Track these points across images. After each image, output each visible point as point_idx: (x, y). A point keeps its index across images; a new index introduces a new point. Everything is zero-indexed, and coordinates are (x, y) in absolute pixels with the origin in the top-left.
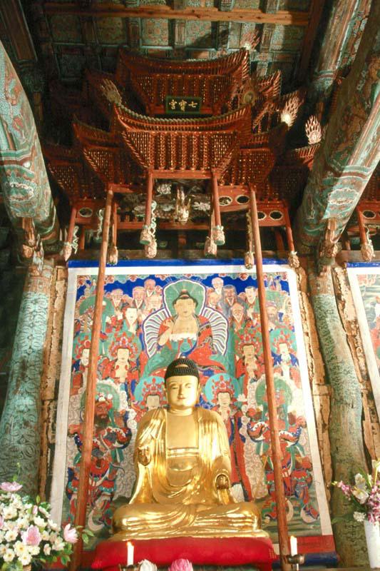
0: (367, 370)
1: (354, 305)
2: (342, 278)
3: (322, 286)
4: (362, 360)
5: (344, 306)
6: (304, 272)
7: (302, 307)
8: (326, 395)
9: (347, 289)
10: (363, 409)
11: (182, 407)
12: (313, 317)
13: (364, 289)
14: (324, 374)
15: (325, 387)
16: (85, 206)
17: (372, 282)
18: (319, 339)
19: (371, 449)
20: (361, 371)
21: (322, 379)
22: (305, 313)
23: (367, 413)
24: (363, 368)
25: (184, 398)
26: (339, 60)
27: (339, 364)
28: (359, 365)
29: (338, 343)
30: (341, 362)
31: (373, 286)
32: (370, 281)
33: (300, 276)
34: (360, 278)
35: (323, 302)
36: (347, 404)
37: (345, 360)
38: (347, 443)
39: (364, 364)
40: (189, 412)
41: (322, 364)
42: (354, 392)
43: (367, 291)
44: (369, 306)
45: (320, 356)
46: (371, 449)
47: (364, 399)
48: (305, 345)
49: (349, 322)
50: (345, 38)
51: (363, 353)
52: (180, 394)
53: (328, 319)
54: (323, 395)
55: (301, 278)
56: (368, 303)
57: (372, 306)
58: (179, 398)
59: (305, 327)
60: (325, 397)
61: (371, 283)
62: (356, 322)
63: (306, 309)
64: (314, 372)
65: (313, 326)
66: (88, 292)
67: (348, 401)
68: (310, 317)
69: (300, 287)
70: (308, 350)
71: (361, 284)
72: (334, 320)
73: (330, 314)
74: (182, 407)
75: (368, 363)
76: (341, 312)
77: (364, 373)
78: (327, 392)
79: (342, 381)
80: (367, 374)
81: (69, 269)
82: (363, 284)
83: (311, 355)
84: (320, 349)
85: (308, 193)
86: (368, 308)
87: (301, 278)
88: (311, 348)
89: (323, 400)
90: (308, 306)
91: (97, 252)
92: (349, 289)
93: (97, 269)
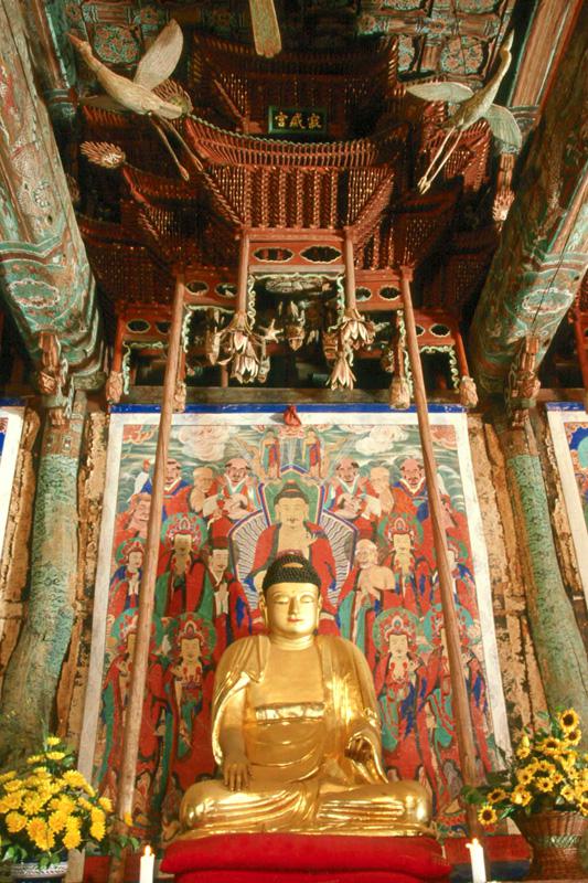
0: (94, 581)
1: (104, 474)
2: (97, 431)
3: (54, 442)
4: (91, 564)
5: (87, 476)
6: (38, 421)
7: (18, 475)
8: (17, 618)
9: (102, 449)
10: (70, 643)
11: (292, 635)
12: (33, 492)
13: (129, 448)
14: (24, 585)
15: (20, 606)
16: (139, 316)
17: (147, 437)
18: (32, 529)
19: (64, 709)
20: (86, 581)
21: (19, 592)
22: (21, 484)
23: (76, 651)
24: (90, 577)
25: (297, 620)
26: (64, 71)
27: (42, 569)
28: (84, 571)
29: (52, 532)
30: (46, 565)
31: (146, 444)
32: (143, 435)
33: (32, 425)
34: (129, 430)
35: (49, 468)
36: (36, 633)
37: (53, 563)
38: (17, 698)
39: (93, 571)
40: (304, 643)
41: (25, 568)
42: (52, 615)
43: (133, 451)
44: (127, 475)
45: (26, 554)
46: (64, 709)
47: (75, 628)
48: (6, 535)
49: (90, 501)
50: (54, 35)
51: (96, 552)
52: (291, 612)
53: (48, 495)
54: (12, 618)
55: (30, 430)
56: (127, 471)
57: (133, 476)
58: (290, 620)
59: (14, 508)
60: (14, 621)
61: (145, 438)
62: (100, 502)
63: (25, 481)
64: (8, 579)
65: (29, 506)
66: (452, 454)
67: (39, 629)
68: (27, 492)
69: (25, 443)
70: (7, 544)
71: (127, 439)
72: (59, 498)
73: (55, 486)
74: (292, 635)
75: (98, 571)
76: (80, 484)
77: (89, 585)
78: (20, 613)
79: (39, 596)
80: (93, 587)
81: (113, 416)
82: (130, 440)
83: (10, 553)
84: (29, 544)
85: (485, 295)
86: (124, 480)
87: (30, 430)
88: (14, 543)
89: (9, 627)
90: (29, 473)
91: (386, 392)
92: (106, 448)
93: (158, 415)
